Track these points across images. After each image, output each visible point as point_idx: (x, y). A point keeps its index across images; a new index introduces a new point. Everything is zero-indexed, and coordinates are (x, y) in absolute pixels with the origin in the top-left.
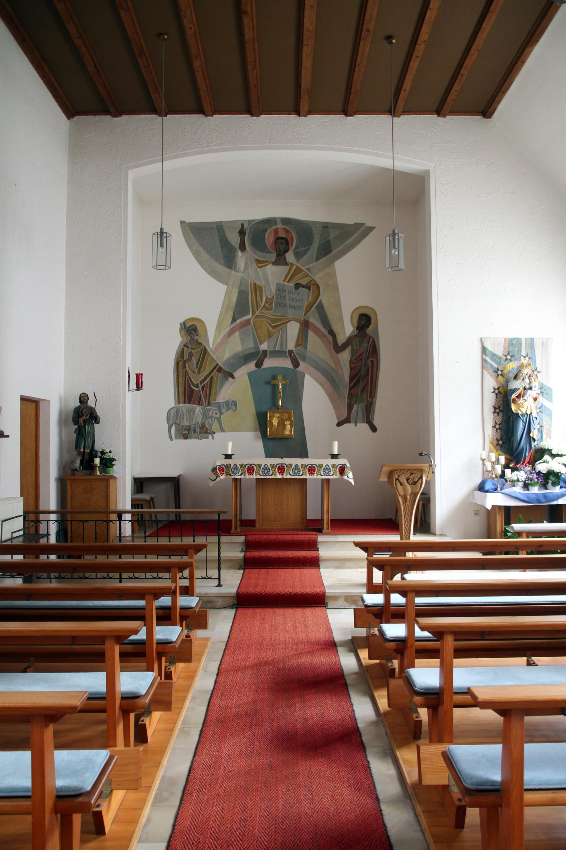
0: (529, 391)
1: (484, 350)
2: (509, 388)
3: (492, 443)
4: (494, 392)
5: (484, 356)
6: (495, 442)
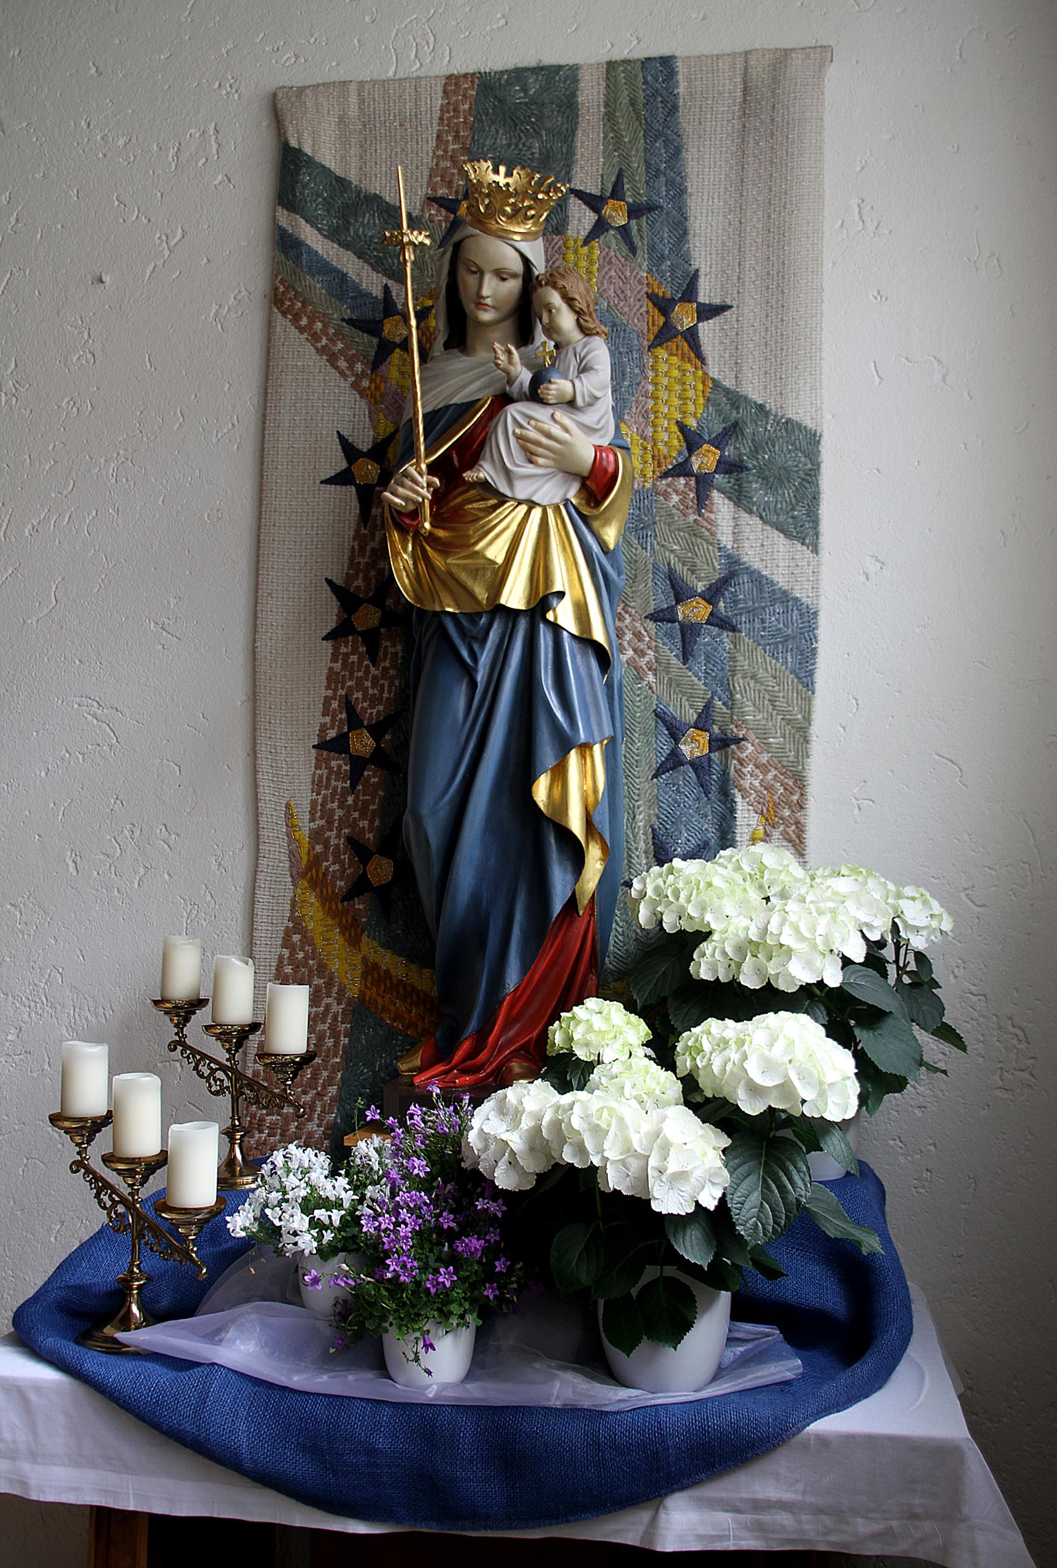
4: (341, 479)
5: (284, 218)
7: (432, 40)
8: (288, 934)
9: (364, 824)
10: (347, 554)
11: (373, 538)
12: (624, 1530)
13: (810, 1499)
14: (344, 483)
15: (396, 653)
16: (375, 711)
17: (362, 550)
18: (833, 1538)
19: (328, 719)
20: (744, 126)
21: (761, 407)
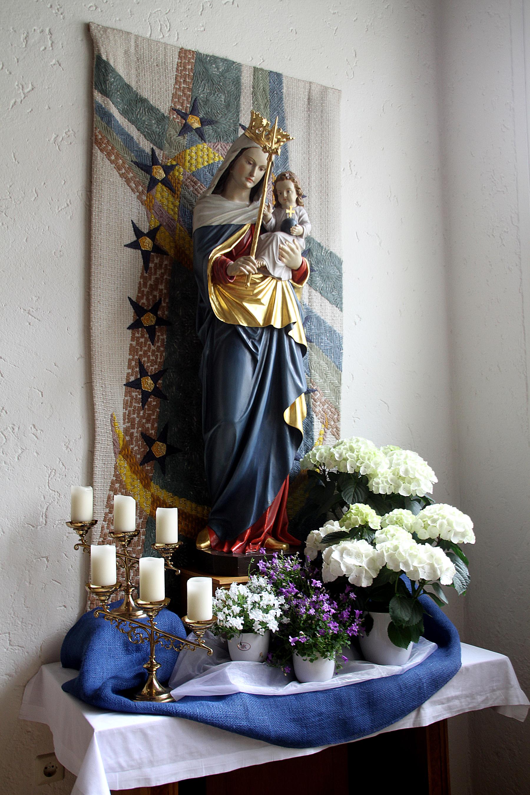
0: (281, 235)
1: (99, 73)
2: (196, 226)
3: (123, 451)
4: (134, 245)
5: (98, 97)
6: (137, 448)
7: (168, 25)
8: (113, 483)
9: (149, 425)
10: (137, 285)
11: (150, 279)
12: (407, 723)
13: (464, 693)
14: (135, 248)
15: (164, 339)
16: (153, 368)
17: (145, 285)
18: (470, 706)
19: (130, 371)
20: (309, 116)
21: (319, 244)
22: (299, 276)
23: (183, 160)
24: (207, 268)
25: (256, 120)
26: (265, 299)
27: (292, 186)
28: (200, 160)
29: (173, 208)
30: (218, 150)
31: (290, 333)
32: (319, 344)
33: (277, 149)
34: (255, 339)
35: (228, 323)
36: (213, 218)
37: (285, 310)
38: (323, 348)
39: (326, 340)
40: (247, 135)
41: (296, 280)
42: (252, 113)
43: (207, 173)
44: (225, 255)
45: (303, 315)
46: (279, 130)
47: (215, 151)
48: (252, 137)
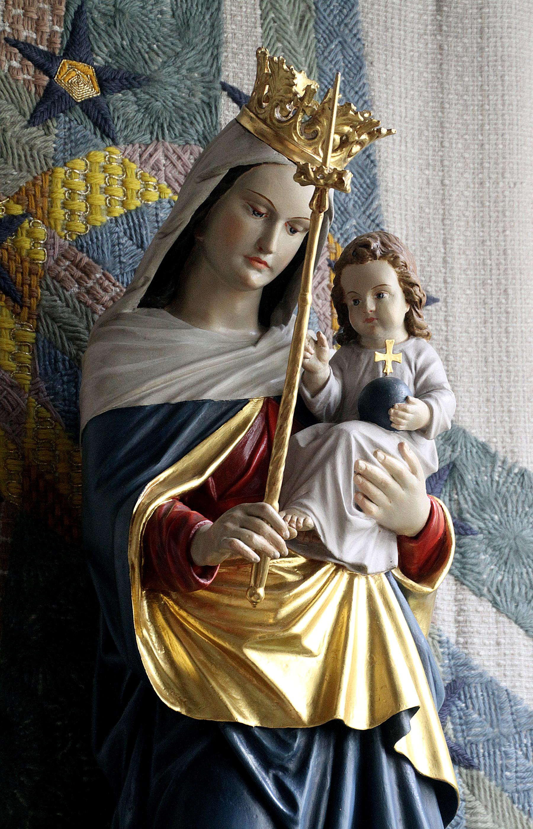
0: (359, 432)
2: (91, 408)
20: (441, 48)
21: (484, 448)
22: (421, 557)
23: (46, 201)
24: (127, 542)
25: (271, 72)
26: (316, 635)
27: (390, 278)
28: (100, 199)
29: (14, 349)
30: (156, 168)
31: (400, 746)
32: (497, 772)
33: (341, 175)
34: (285, 769)
35: (198, 716)
36: (145, 382)
37: (380, 670)
38: (510, 787)
39: (522, 760)
40: (248, 126)
41: (414, 568)
42: (261, 57)
43: (124, 240)
44: (183, 498)
45: (440, 677)
46: (345, 108)
47: (148, 169)
48: (262, 134)
